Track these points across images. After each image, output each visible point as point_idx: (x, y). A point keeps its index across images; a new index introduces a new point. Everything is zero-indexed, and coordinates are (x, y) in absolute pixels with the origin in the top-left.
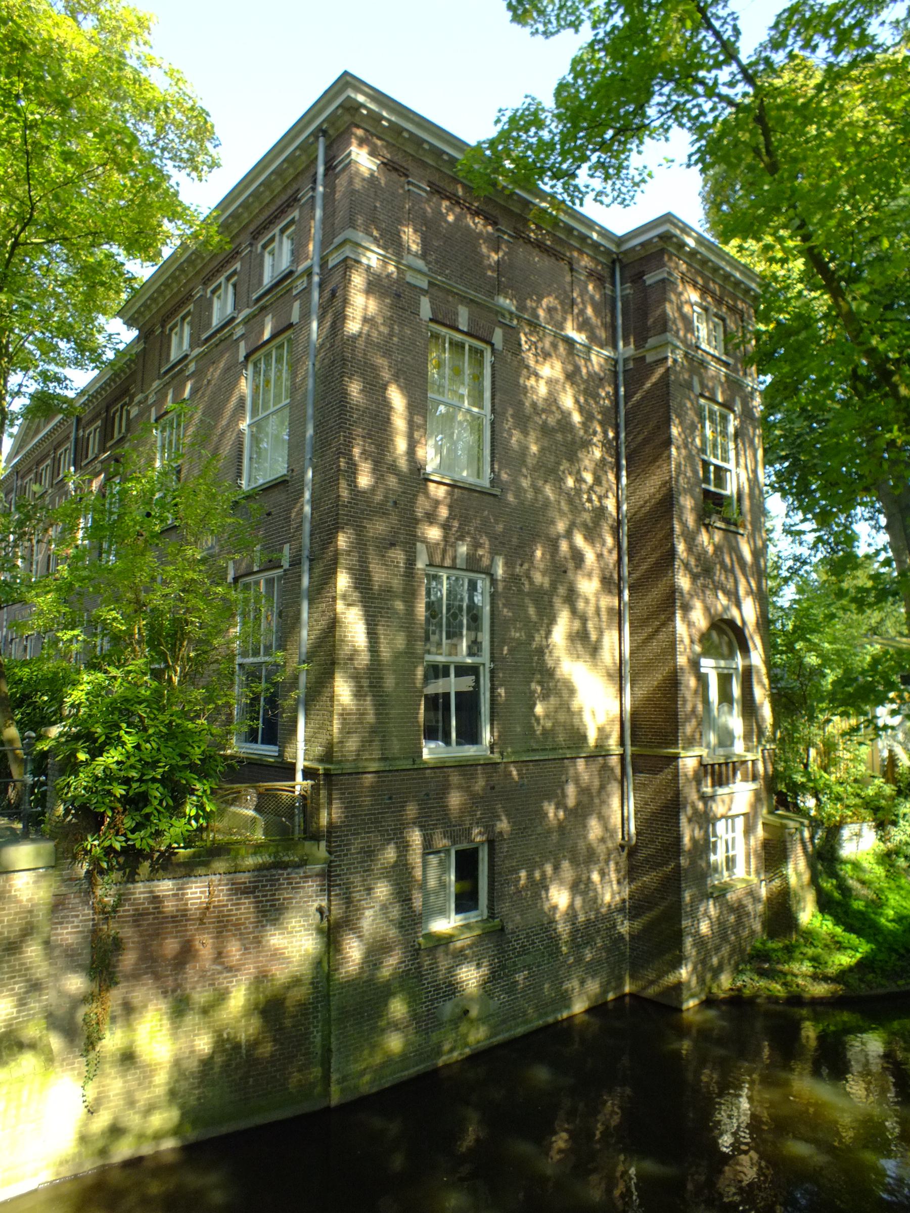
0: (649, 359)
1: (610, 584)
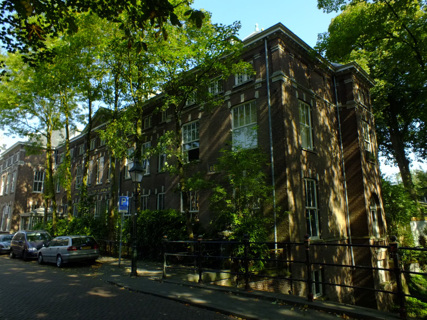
0: (348, 108)
1: (341, 181)
